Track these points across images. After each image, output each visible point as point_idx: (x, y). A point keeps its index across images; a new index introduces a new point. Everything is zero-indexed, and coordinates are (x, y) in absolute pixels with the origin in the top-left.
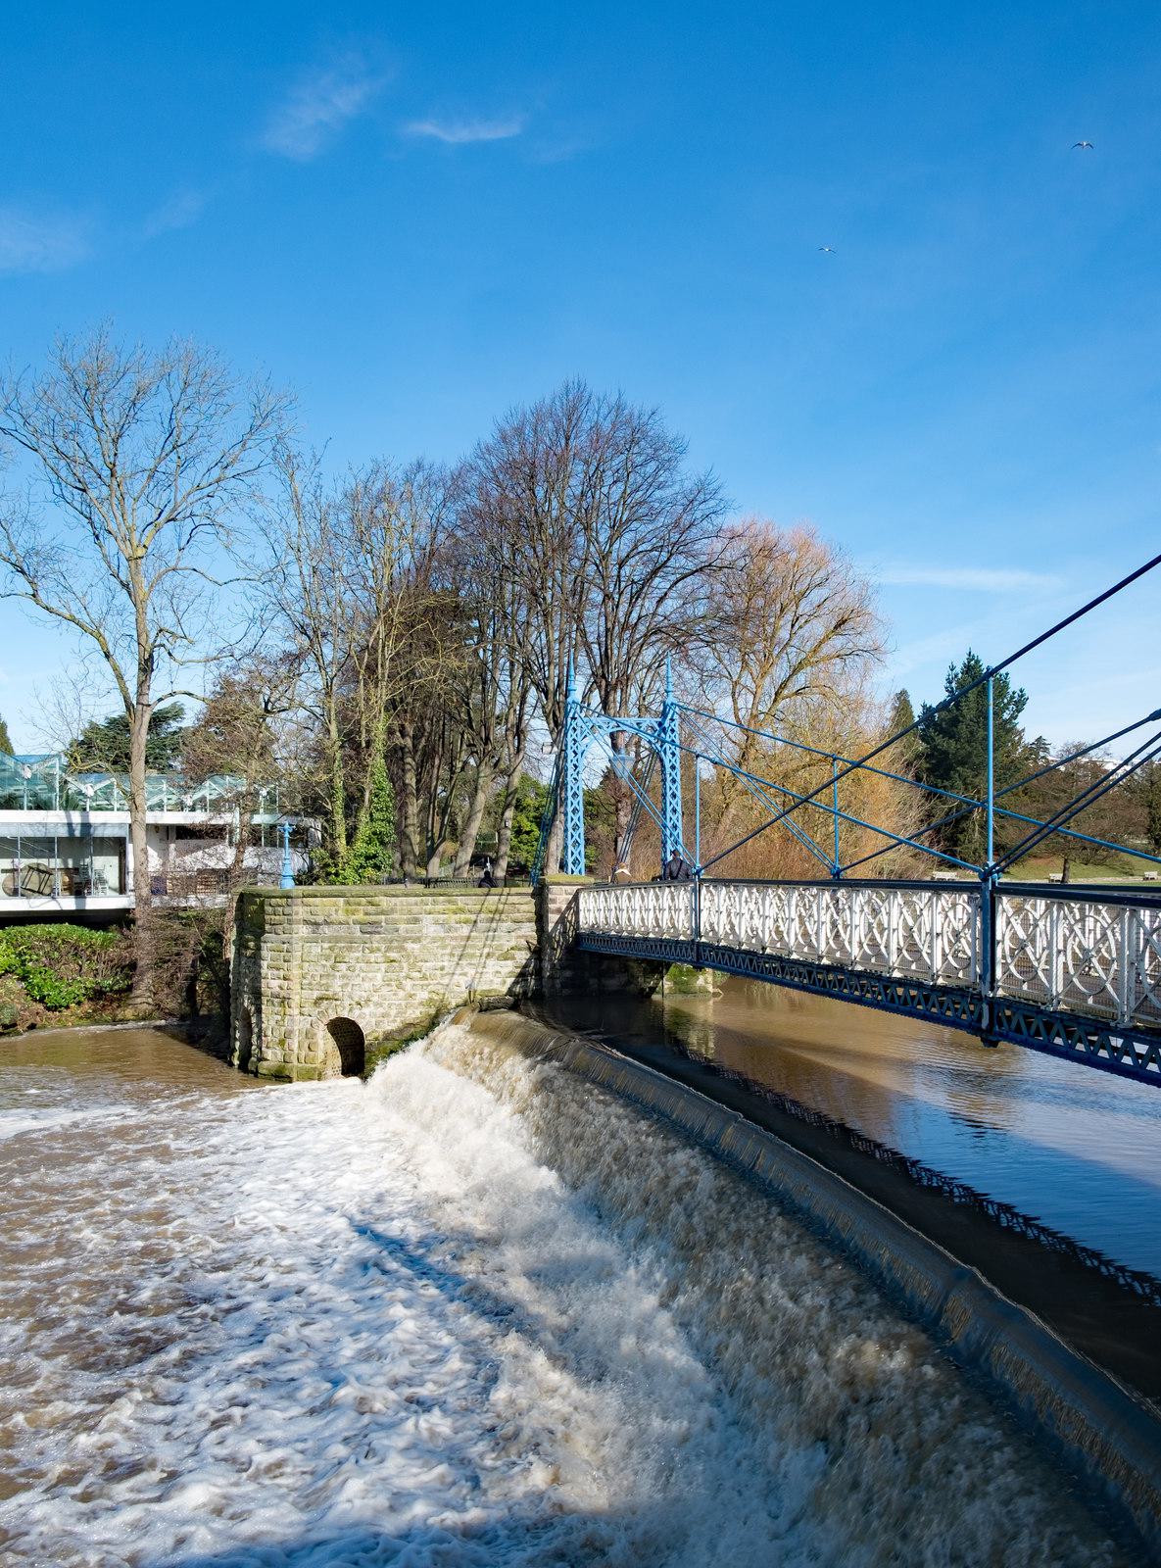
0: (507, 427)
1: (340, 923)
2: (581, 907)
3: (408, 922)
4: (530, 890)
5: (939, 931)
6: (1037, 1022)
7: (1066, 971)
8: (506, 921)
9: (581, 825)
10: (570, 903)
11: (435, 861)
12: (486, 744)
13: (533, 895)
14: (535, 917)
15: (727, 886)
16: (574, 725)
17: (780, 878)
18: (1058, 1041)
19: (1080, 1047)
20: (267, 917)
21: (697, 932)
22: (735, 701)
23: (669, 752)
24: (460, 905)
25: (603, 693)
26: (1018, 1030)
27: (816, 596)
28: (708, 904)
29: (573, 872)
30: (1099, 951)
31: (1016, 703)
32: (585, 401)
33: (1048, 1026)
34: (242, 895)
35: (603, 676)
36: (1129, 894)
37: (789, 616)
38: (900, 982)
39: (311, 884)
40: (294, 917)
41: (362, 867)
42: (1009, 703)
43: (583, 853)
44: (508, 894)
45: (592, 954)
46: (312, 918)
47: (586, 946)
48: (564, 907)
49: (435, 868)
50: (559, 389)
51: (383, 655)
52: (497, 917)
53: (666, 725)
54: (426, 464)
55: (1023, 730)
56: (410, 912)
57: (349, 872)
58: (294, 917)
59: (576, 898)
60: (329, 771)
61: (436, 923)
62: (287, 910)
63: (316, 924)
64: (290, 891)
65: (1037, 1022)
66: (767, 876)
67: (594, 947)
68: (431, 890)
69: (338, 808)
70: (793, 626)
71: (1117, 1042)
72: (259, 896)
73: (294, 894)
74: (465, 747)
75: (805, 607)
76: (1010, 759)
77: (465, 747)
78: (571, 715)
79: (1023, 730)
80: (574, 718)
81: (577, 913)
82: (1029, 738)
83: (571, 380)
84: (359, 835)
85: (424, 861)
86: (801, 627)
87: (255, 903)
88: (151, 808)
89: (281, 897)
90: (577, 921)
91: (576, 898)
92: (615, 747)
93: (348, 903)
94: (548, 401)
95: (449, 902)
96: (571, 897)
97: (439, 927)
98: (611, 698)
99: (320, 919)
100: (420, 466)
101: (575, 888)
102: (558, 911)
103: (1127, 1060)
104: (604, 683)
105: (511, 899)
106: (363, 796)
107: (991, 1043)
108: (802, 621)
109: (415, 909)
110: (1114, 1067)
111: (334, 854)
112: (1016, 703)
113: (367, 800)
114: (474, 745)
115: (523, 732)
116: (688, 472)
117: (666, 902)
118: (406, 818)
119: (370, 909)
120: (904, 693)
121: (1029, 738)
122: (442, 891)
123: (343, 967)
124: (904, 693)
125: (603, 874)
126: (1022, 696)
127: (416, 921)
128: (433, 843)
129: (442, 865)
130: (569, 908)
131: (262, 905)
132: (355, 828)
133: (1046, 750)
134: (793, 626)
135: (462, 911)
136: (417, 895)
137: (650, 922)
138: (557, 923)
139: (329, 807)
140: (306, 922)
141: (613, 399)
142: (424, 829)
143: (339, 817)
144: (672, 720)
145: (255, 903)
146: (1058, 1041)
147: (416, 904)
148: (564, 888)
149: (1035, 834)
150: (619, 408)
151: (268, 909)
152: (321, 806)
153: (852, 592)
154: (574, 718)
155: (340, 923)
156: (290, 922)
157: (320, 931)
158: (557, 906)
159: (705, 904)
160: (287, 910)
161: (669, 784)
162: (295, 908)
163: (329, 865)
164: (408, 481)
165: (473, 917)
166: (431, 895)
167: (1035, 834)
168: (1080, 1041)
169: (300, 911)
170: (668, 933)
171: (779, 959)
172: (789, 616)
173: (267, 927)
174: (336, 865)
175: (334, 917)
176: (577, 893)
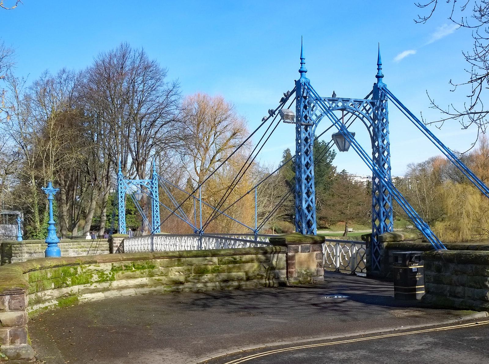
0: (98, 60)
1: (40, 253)
2: (125, 245)
3: (64, 251)
4: (107, 240)
5: (339, 255)
8: (99, 250)
10: (121, 244)
11: (76, 229)
12: (95, 181)
13: (108, 241)
14: (109, 249)
16: (121, 182)
20: (13, 251)
22: (195, 163)
23: (154, 191)
24: (82, 245)
25: (136, 166)
27: (224, 123)
28: (155, 242)
29: (122, 233)
31: (332, 156)
32: (128, 51)
34: (2, 244)
35: (136, 160)
37: (213, 132)
39: (26, 239)
40: (23, 251)
41: (46, 233)
42: (329, 156)
43: (125, 227)
44: (100, 241)
46: (29, 251)
48: (119, 245)
49: (75, 233)
50: (119, 46)
51: (52, 154)
52: (96, 249)
53: (153, 182)
54: (67, 70)
55: (336, 167)
56: (64, 248)
57: (41, 235)
58: (23, 251)
59: (123, 242)
60: (33, 197)
61: (74, 251)
62: (20, 249)
63: (31, 253)
64: (21, 242)
68: (72, 240)
69: (36, 211)
70: (215, 135)
72: (9, 244)
73: (23, 243)
74: (86, 182)
75: (219, 128)
76: (330, 180)
77: (86, 182)
78: (120, 179)
79: (336, 167)
80: (121, 180)
81: (123, 247)
82: (339, 170)
83: (123, 43)
84: (45, 221)
85: (71, 229)
86: (218, 136)
87: (8, 247)
89: (18, 244)
90: (123, 250)
91: (123, 242)
93: (42, 246)
94: (115, 51)
95: (78, 244)
96: (121, 242)
97: (75, 253)
98: (140, 168)
99: (32, 251)
100: (64, 71)
101: (123, 238)
102: (117, 246)
104: (137, 162)
105: (101, 243)
106: (45, 206)
108: (218, 133)
109: (66, 247)
111: (35, 228)
112: (332, 156)
113: (47, 208)
114: (90, 181)
115: (109, 177)
116: (168, 81)
117: (139, 243)
118: (62, 213)
120: (288, 150)
121: (339, 170)
122: (76, 240)
124: (288, 150)
126: (334, 153)
127: (67, 251)
128: (75, 222)
129: (79, 230)
130: (120, 245)
131: (11, 247)
132: (43, 218)
134: (215, 135)
135: (83, 247)
136: (67, 242)
137: (143, 248)
138: (117, 251)
139: (33, 211)
140: (27, 253)
141: (140, 51)
142: (71, 216)
143: (37, 214)
144: (155, 180)
145: (8, 247)
147: (67, 245)
148: (118, 238)
149: (204, 225)
150: (142, 55)
151: (13, 248)
152: (29, 210)
153: (239, 120)
154: (121, 180)
155: (40, 253)
156: (21, 253)
157: (33, 255)
158: (116, 245)
159: (154, 242)
160: (20, 249)
162: (23, 248)
163: (33, 232)
164: (60, 77)
165: (88, 249)
166: (72, 242)
167: (204, 225)
169: (25, 249)
172: (213, 132)
173: (13, 255)
174: (36, 232)
175: (37, 250)
176: (123, 240)
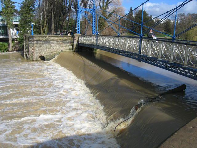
6: (147, 59)
7: (151, 51)
9: (80, 28)
15: (74, 39)
17: (184, 30)
18: (149, 61)
19: (152, 62)
21: (97, 43)
26: (144, 60)
30: (156, 48)
33: (148, 59)
36: (164, 40)
38: (127, 52)
45: (81, 46)
47: (80, 45)
63: (37, 41)
65: (147, 59)
66: (113, 35)
67: (81, 45)
71: (158, 62)
88: (14, 22)
92: (85, 13)
103: (159, 65)
107: (140, 61)
110: (157, 66)
119: (46, 38)
120: (131, 7)
123: (42, 48)
124: (131, 7)
125: (83, 34)
133: (152, 17)
140: (36, 40)
146: (149, 61)
161: (94, 20)
168: (174, 68)
170: (117, 48)
171: (118, 50)
